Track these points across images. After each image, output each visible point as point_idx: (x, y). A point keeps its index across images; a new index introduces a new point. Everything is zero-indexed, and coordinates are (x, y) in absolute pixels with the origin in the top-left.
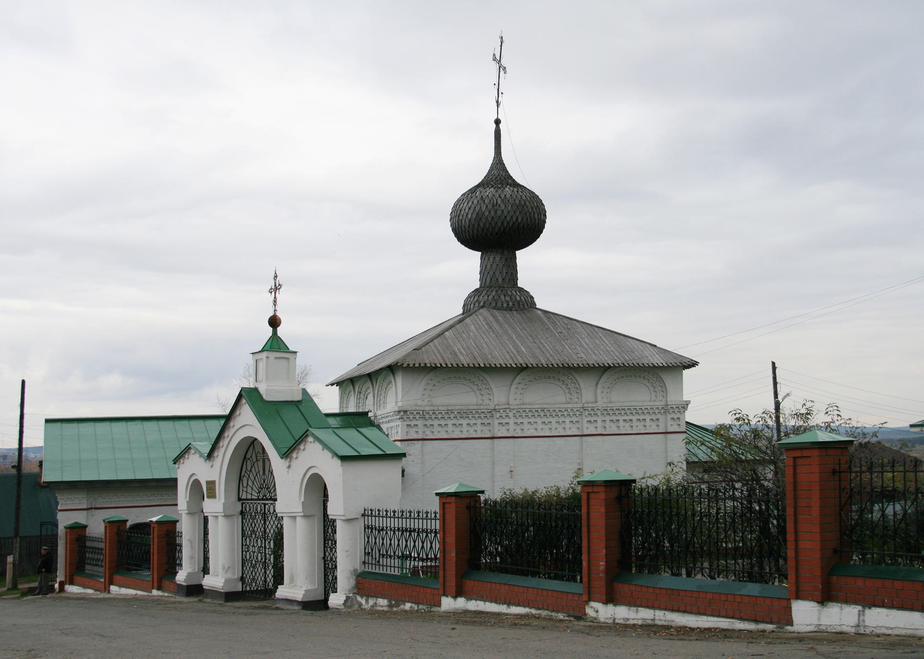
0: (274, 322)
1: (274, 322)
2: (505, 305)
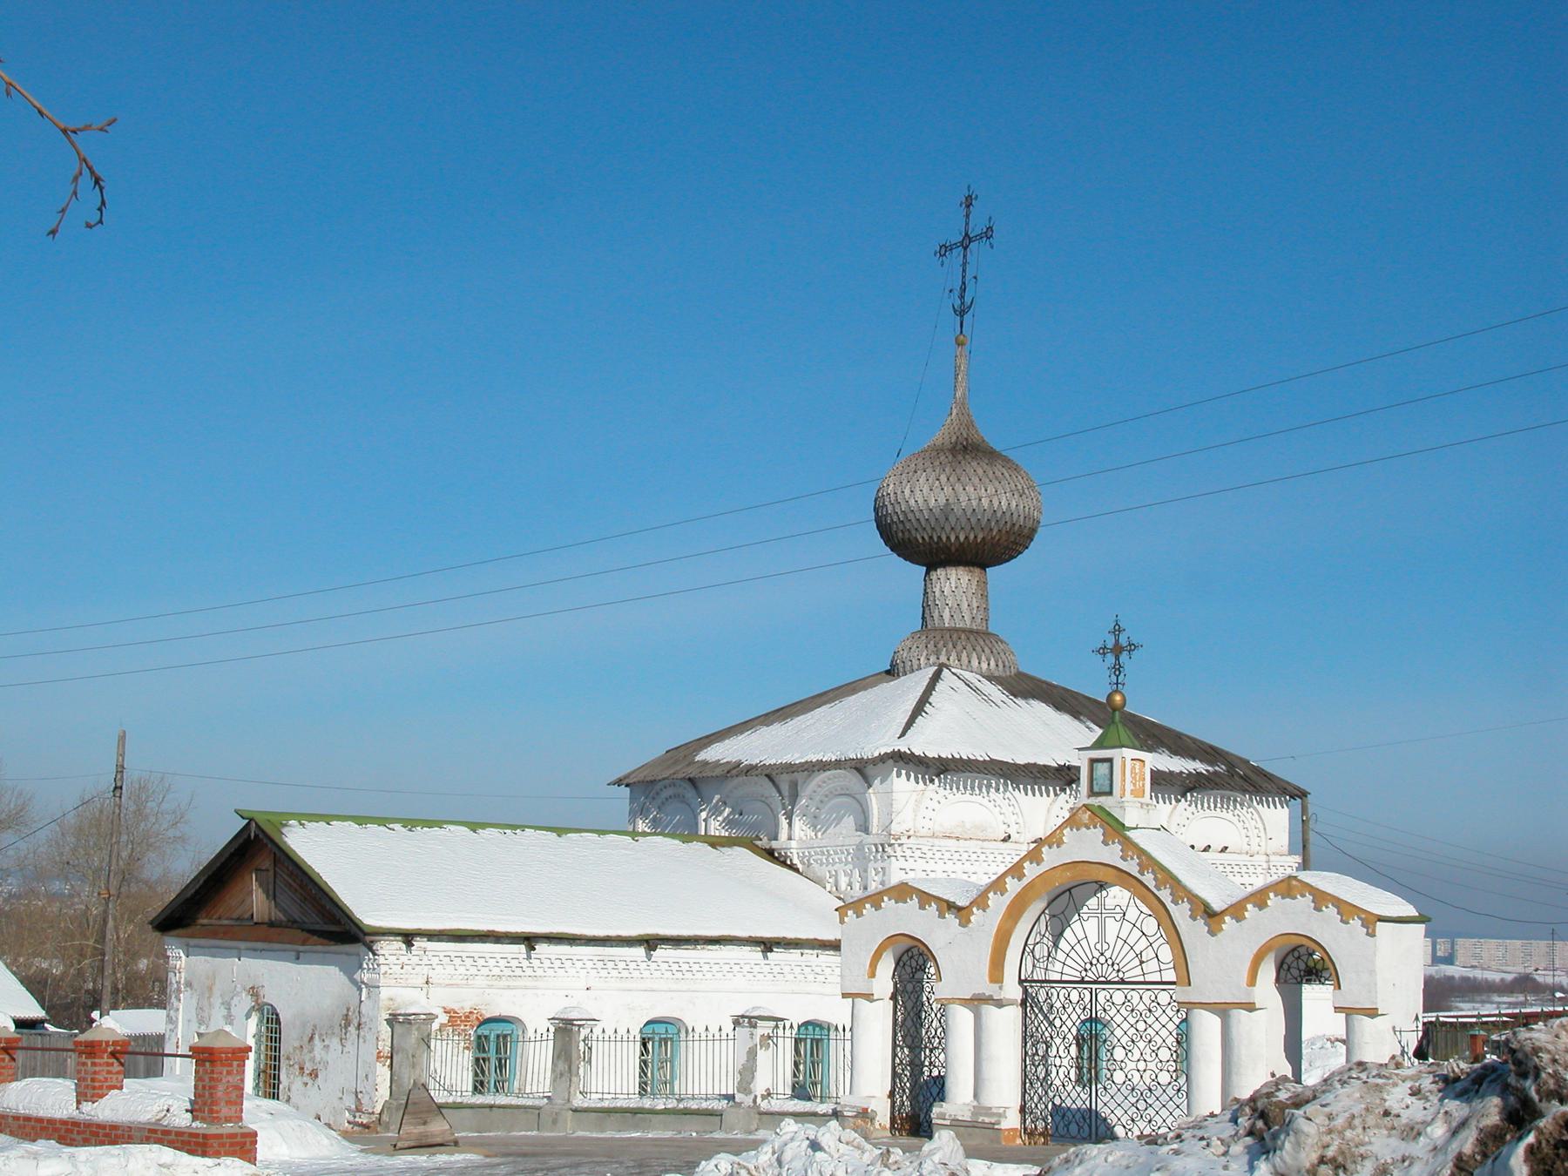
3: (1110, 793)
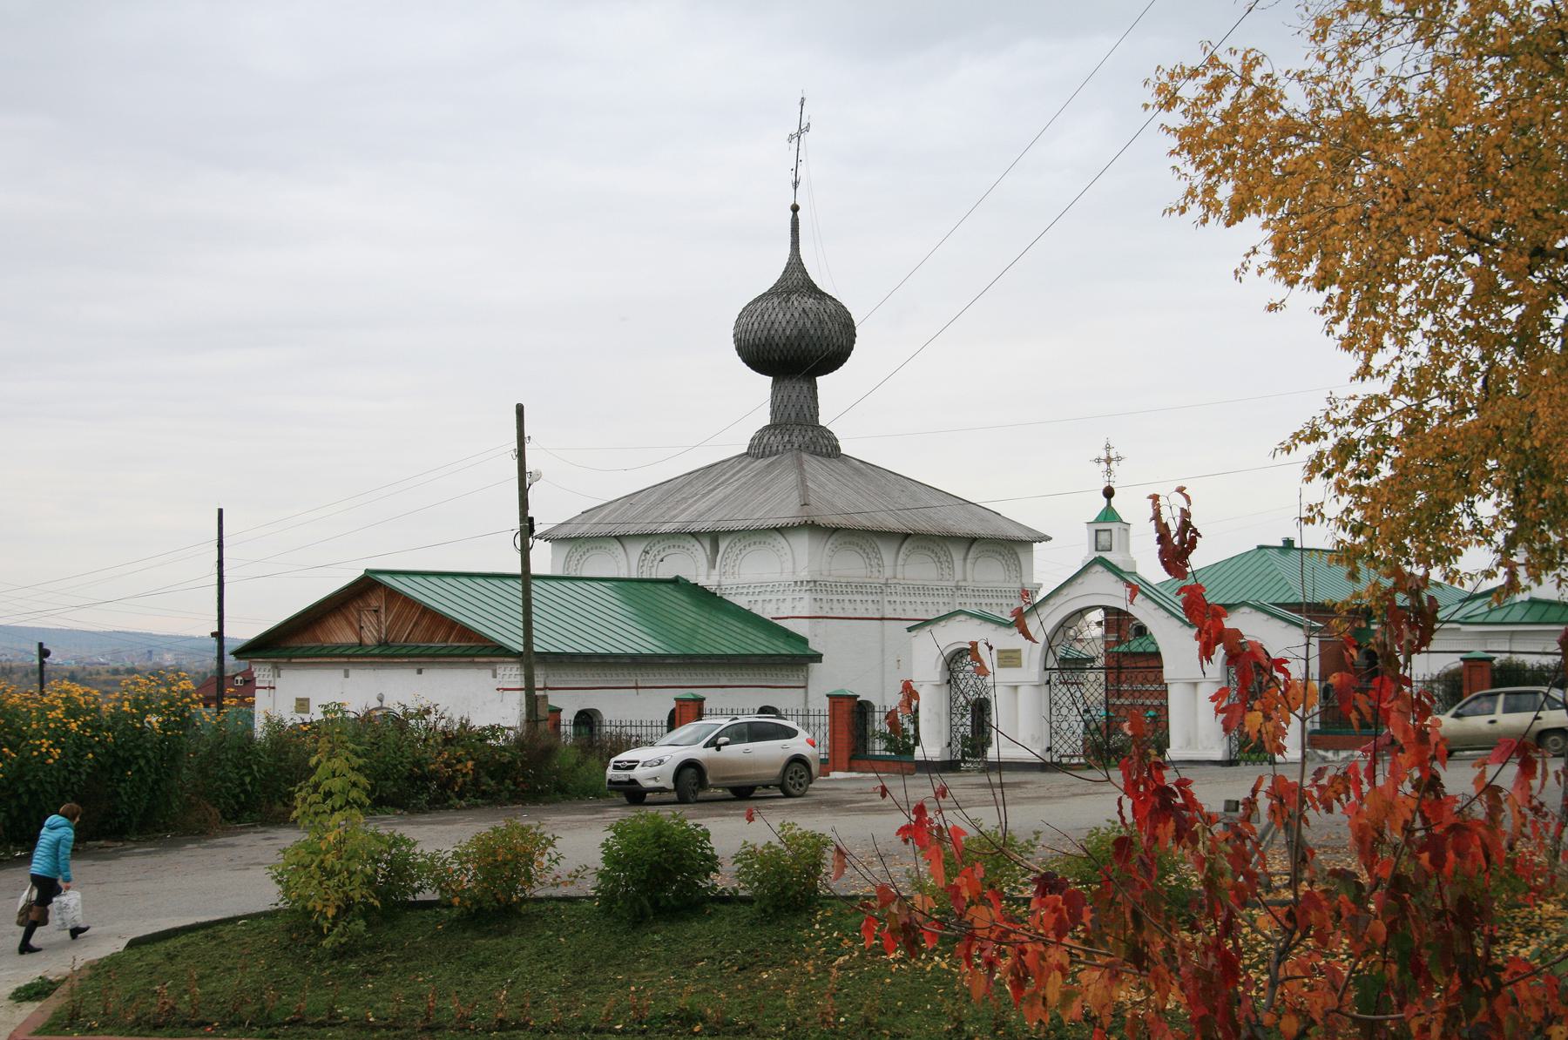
0: (1109, 493)
1: (1109, 493)
2: (824, 450)
3: (1110, 550)
